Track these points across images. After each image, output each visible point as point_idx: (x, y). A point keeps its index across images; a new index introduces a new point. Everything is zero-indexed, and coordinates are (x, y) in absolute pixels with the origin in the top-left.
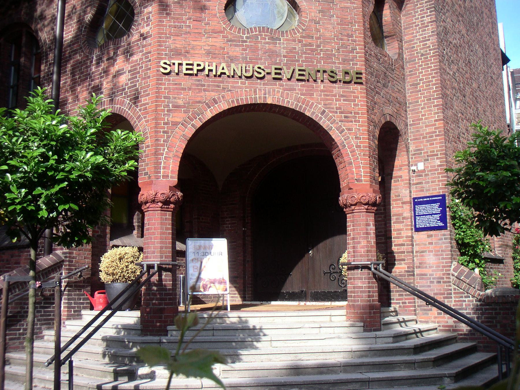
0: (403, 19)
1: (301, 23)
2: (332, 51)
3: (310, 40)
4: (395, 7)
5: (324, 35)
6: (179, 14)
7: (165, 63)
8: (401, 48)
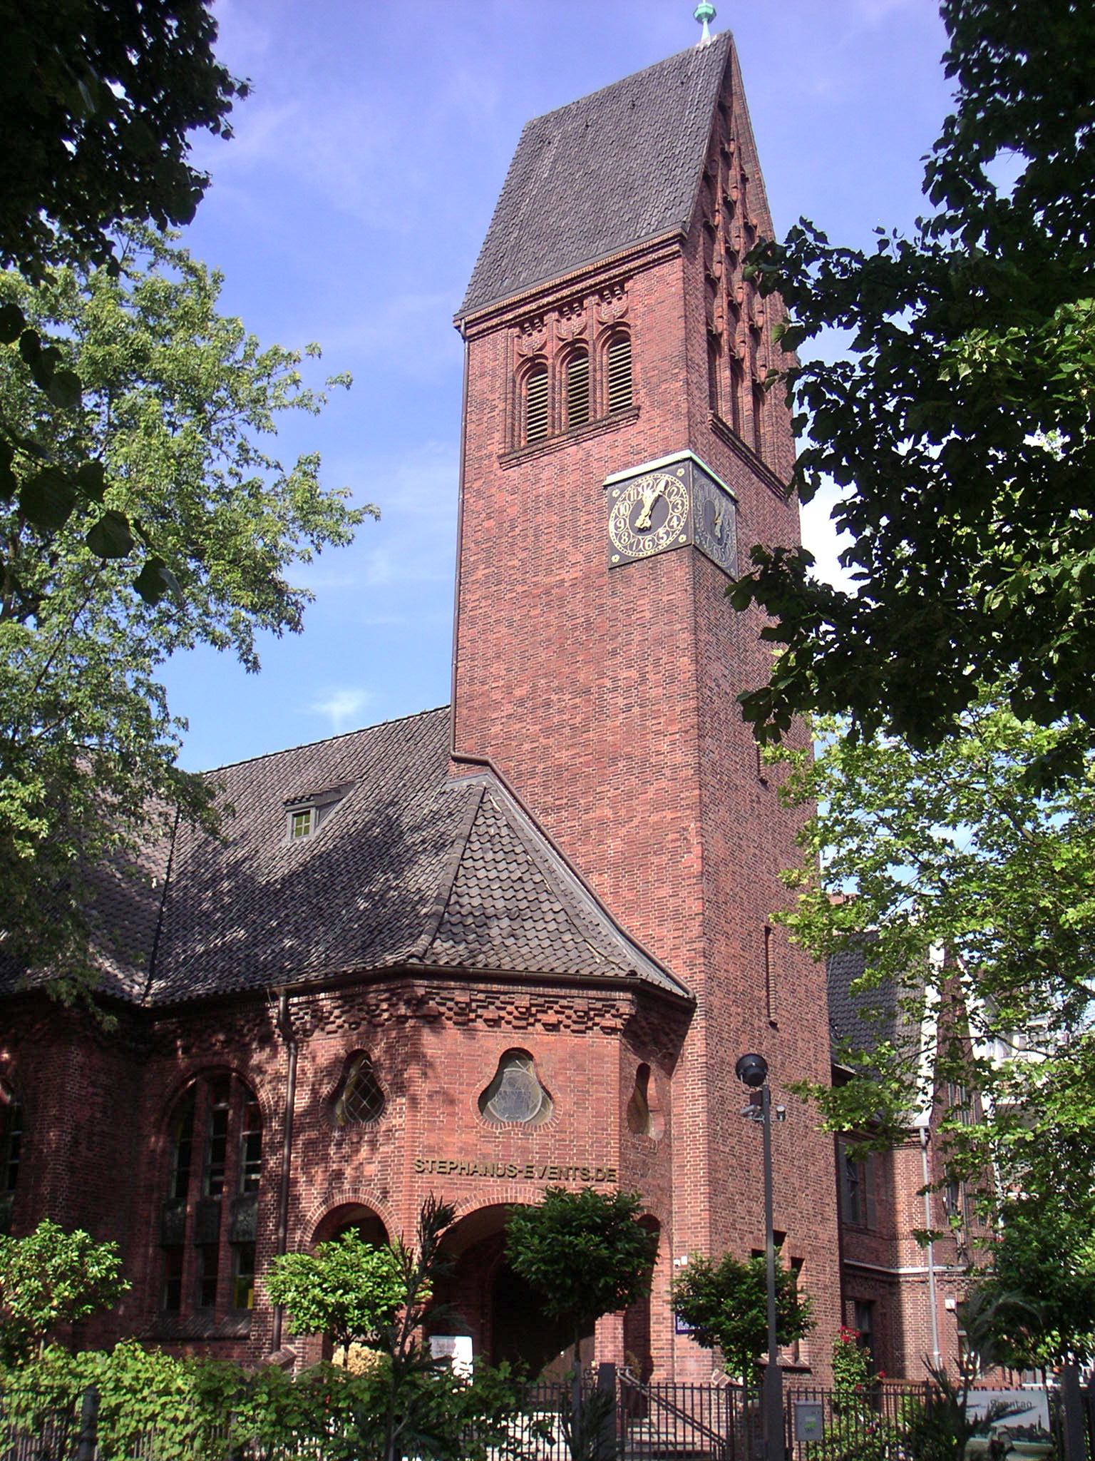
3: (563, 1135)
8: (668, 1123)
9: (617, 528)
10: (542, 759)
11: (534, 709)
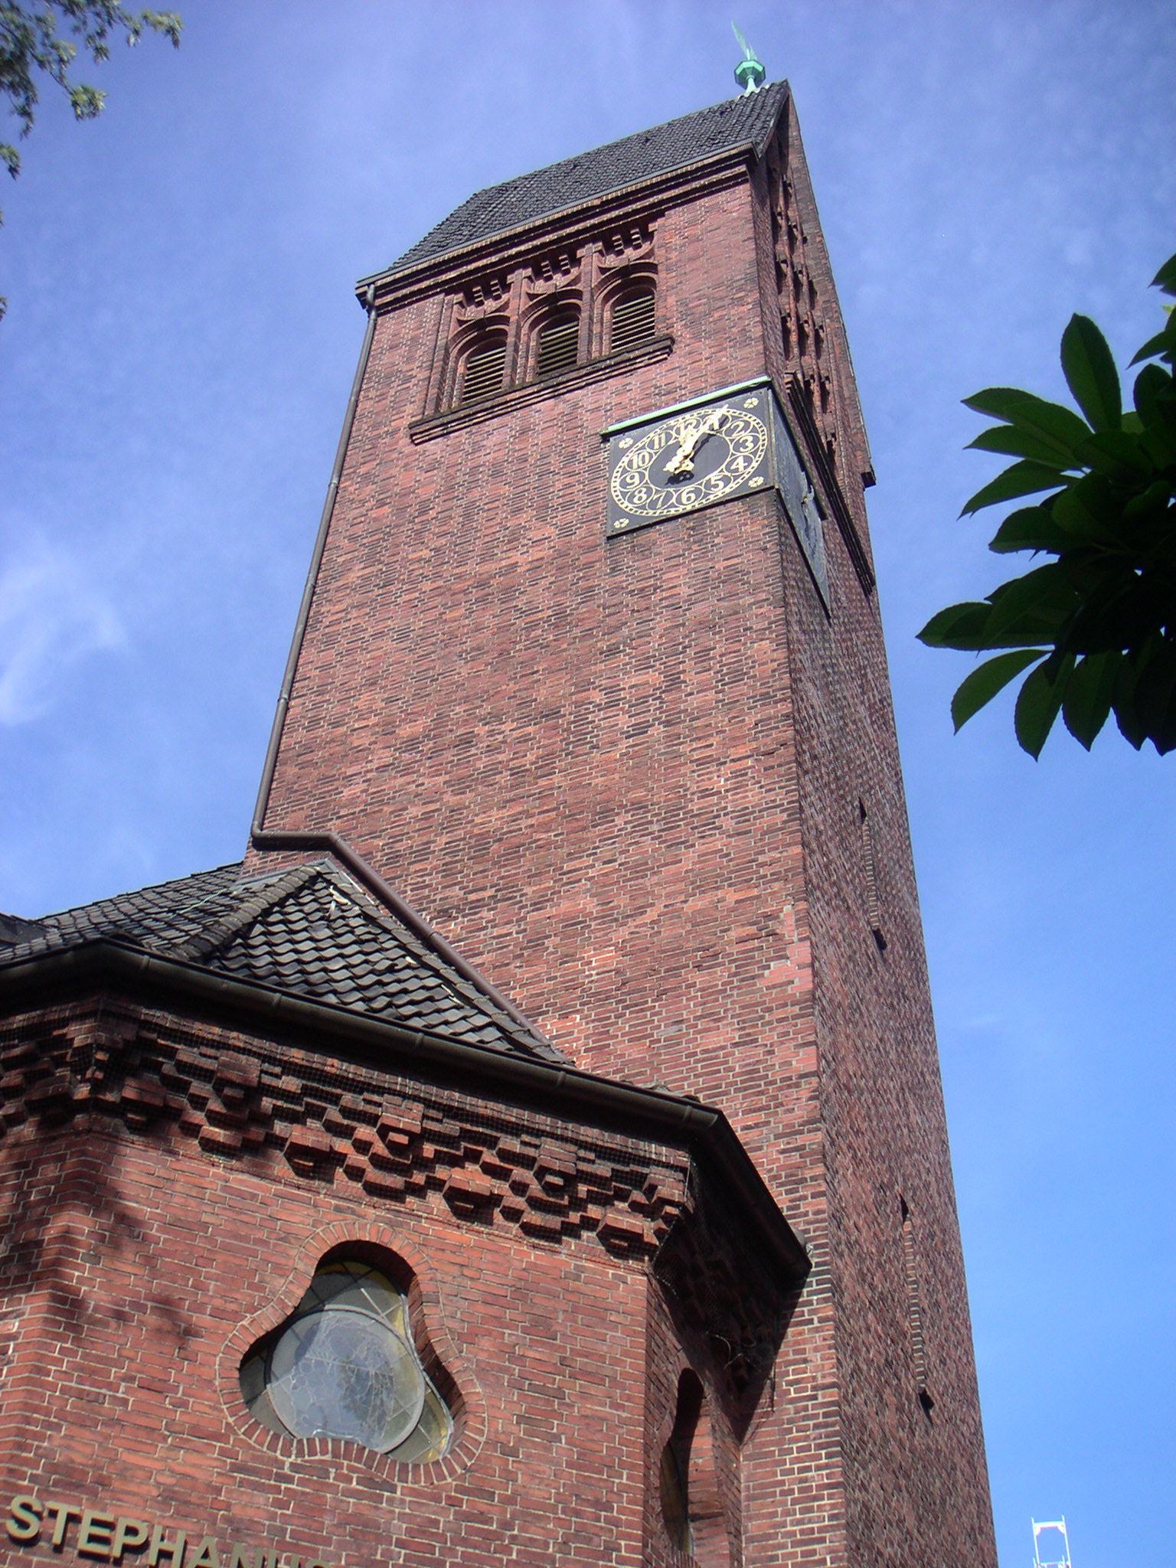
0: (745, 1468)
1: (461, 1446)
2: (546, 1545)
3: (482, 1504)
4: (726, 1431)
5: (527, 1493)
6: (99, 1359)
7: (26, 1507)
9: (624, 484)
10: (445, 828)
11: (437, 751)
